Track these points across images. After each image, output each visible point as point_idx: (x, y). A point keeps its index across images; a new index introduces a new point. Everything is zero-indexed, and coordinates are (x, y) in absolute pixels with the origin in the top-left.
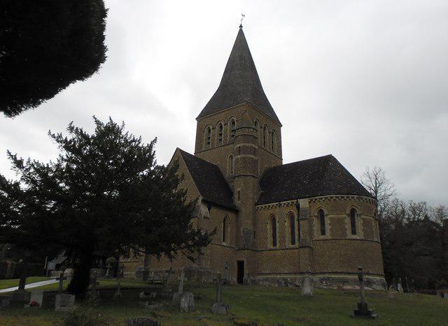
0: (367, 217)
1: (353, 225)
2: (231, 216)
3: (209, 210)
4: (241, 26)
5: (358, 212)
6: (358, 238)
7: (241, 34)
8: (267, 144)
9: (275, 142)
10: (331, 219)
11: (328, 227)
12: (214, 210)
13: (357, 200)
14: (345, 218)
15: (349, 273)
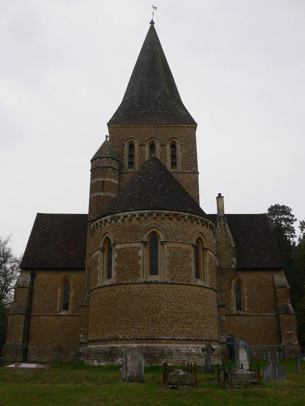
0: (127, 245)
4: (152, 23)
10: (118, 251)
11: (114, 264)
12: (42, 276)
13: (113, 222)
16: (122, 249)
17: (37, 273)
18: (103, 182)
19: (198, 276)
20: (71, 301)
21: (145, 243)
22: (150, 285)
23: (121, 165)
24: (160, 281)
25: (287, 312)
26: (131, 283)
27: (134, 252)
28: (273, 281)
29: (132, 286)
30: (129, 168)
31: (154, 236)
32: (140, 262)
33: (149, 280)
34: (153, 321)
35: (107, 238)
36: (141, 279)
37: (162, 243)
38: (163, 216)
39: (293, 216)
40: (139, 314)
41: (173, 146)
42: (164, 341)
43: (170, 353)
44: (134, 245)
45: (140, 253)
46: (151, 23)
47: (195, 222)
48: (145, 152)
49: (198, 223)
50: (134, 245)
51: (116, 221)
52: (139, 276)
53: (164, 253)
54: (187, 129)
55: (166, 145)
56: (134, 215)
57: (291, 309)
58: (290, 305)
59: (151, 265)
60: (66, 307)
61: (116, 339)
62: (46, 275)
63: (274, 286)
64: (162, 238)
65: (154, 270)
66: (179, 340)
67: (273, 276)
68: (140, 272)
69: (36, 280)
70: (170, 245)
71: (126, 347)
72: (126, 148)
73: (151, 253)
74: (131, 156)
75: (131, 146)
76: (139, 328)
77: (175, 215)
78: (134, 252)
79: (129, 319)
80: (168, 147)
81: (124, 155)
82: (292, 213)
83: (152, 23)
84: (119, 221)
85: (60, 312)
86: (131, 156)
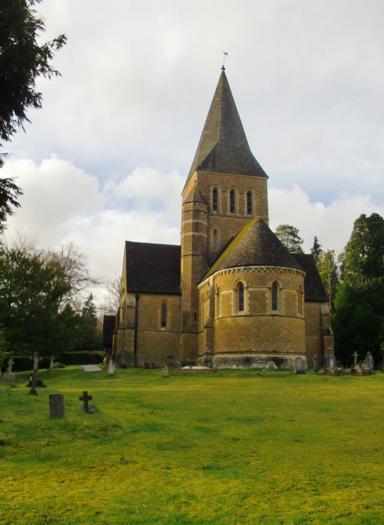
0: (258, 289)
1: (241, 300)
2: (171, 300)
3: (137, 299)
4: (223, 69)
5: (245, 284)
6: (242, 314)
7: (223, 78)
8: (237, 208)
9: (255, 203)
12: (145, 299)
14: (231, 293)
15: (230, 353)
16: (253, 291)
17: (141, 295)
18: (197, 223)
19: (275, 307)
20: (168, 320)
21: (270, 288)
22: (274, 317)
23: (209, 209)
24: (280, 314)
25: (328, 333)
26: (261, 316)
27: (263, 294)
28: (320, 311)
29: (262, 317)
30: (214, 210)
31: (275, 285)
32: (267, 302)
33: (273, 314)
34: (276, 341)
35: (240, 282)
36: (268, 313)
37: (281, 289)
38: (282, 270)
39: (298, 238)
40: (267, 336)
41: (249, 194)
42: (282, 353)
43: (286, 360)
44: (262, 289)
45: (267, 295)
46: (222, 69)
47: (292, 273)
48: (227, 198)
49: (294, 273)
50: (262, 289)
51: (248, 271)
52: (266, 311)
53: (282, 296)
54: (261, 181)
55: (244, 194)
56: (262, 269)
57: (332, 332)
58: (330, 328)
59: (273, 303)
60: (164, 324)
61: (250, 352)
62: (147, 298)
63: (321, 312)
64: (281, 286)
65: (275, 307)
66: (291, 353)
67: (320, 306)
68: (267, 308)
69: (139, 302)
70: (286, 290)
71: (258, 357)
72: (211, 194)
73: (273, 295)
74: (215, 200)
75: (215, 191)
76: (267, 345)
77: (289, 270)
78: (263, 294)
79: (260, 339)
80: (245, 195)
81: (209, 199)
82: (299, 235)
83: (223, 69)
84: (251, 271)
85: (160, 328)
86: (215, 200)
